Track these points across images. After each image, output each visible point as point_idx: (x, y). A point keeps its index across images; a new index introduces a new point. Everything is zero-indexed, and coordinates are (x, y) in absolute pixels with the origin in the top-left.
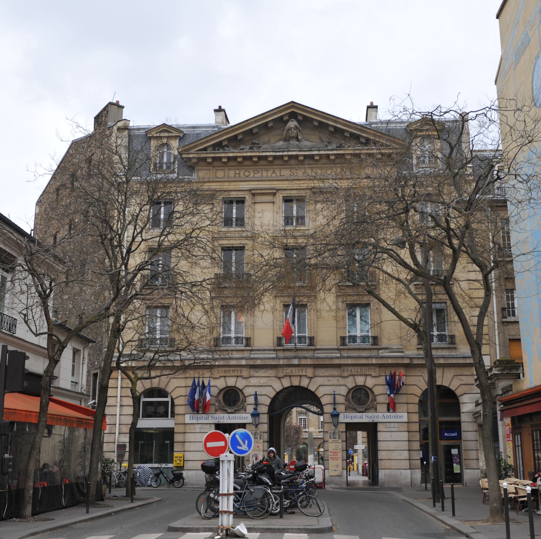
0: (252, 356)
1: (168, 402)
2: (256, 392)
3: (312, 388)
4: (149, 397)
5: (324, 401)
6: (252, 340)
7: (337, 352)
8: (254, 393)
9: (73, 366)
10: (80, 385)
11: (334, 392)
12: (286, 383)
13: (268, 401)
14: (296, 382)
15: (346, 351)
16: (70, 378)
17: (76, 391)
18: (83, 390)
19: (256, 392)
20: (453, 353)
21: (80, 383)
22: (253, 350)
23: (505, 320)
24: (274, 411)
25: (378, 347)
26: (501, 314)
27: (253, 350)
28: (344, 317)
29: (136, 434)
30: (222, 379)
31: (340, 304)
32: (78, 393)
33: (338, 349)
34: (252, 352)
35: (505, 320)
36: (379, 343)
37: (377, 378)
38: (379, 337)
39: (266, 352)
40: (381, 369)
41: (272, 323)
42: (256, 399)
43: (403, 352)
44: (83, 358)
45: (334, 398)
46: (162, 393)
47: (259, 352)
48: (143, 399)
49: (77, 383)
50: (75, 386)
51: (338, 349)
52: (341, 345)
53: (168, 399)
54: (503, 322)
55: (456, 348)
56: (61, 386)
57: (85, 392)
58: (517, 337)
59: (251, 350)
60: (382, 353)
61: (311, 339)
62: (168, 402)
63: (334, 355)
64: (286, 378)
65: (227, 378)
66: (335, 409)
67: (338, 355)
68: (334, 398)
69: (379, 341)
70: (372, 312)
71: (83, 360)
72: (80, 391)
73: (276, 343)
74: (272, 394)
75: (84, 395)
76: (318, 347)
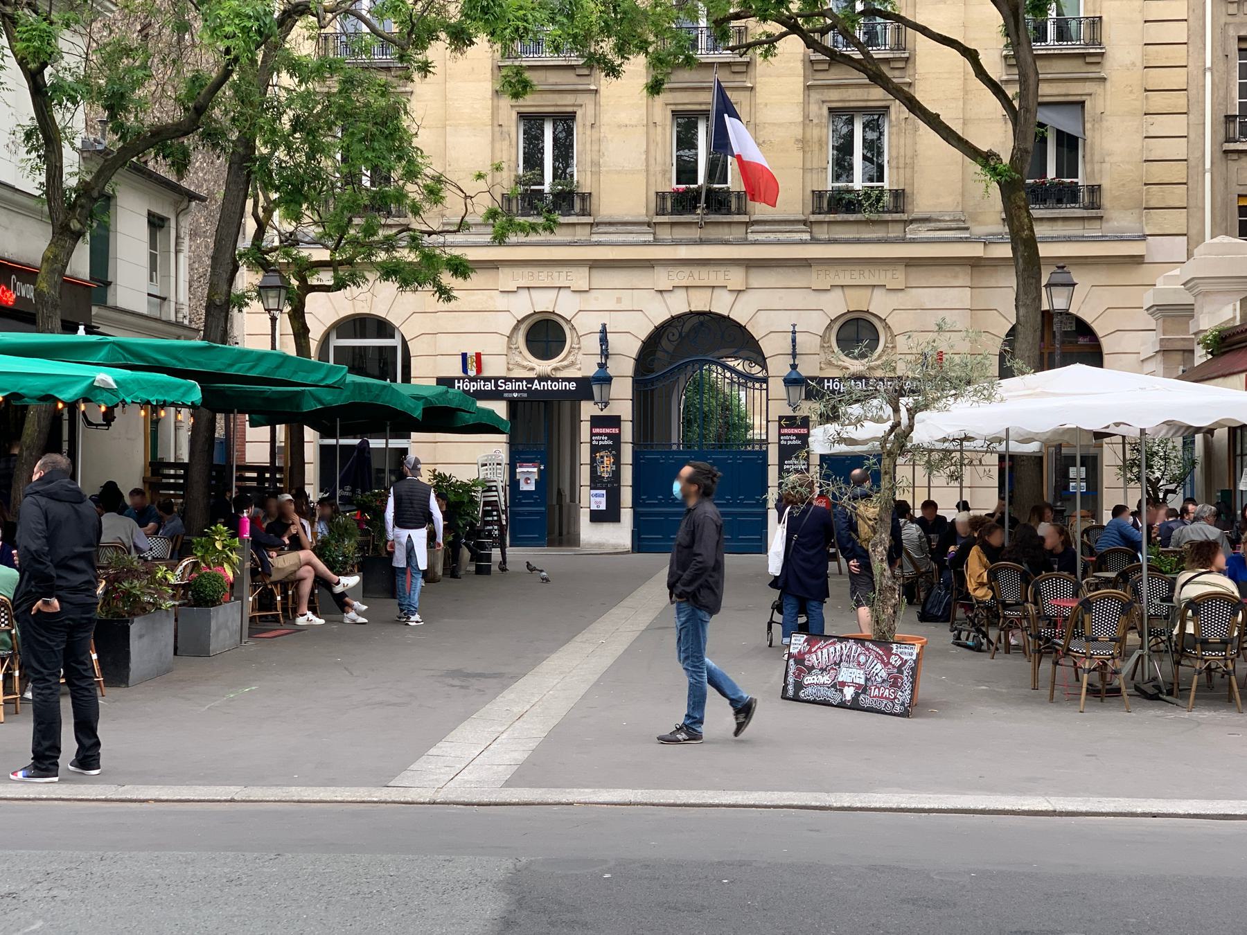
0: (595, 238)
1: (395, 348)
2: (604, 326)
3: (740, 316)
4: (355, 337)
5: (767, 347)
6: (594, 200)
7: (645, 228)
8: (600, 328)
9: (153, 258)
10: (173, 305)
11: (794, 326)
12: (679, 305)
13: (634, 348)
14: (699, 303)
15: (825, 227)
16: (144, 285)
17: (164, 318)
18: (180, 315)
19: (604, 326)
20: (1093, 230)
21: (173, 298)
22: (598, 224)
23: (1232, 146)
24: (652, 371)
25: (905, 217)
26: (1222, 132)
27: (598, 224)
28: (821, 144)
29: (619, 426)
30: (681, 294)
31: (814, 108)
32: (168, 323)
33: (805, 223)
34: (595, 229)
35: (1232, 146)
36: (908, 208)
37: (900, 294)
38: (908, 191)
39: (630, 228)
40: (910, 269)
41: (644, 157)
42: (604, 341)
43: (967, 229)
44: (177, 237)
45: (794, 341)
46: (383, 327)
47: (612, 229)
48: (336, 342)
49: (164, 299)
50: (161, 305)
51: (805, 223)
52: (813, 213)
53: (395, 342)
54: (1226, 152)
55: (1101, 218)
56: (121, 303)
57: (186, 322)
58: (756, 197)
59: (747, 224)
60: (914, 231)
61: (898, 195)
62: (395, 348)
63: (797, 236)
64: (521, 291)
65: (691, 291)
66: (794, 367)
67: (806, 236)
68: (794, 341)
69: (908, 200)
70: (894, 130)
71: (177, 244)
72: (173, 318)
73: (652, 206)
74: (644, 332)
75: (185, 327)
76: (754, 218)
